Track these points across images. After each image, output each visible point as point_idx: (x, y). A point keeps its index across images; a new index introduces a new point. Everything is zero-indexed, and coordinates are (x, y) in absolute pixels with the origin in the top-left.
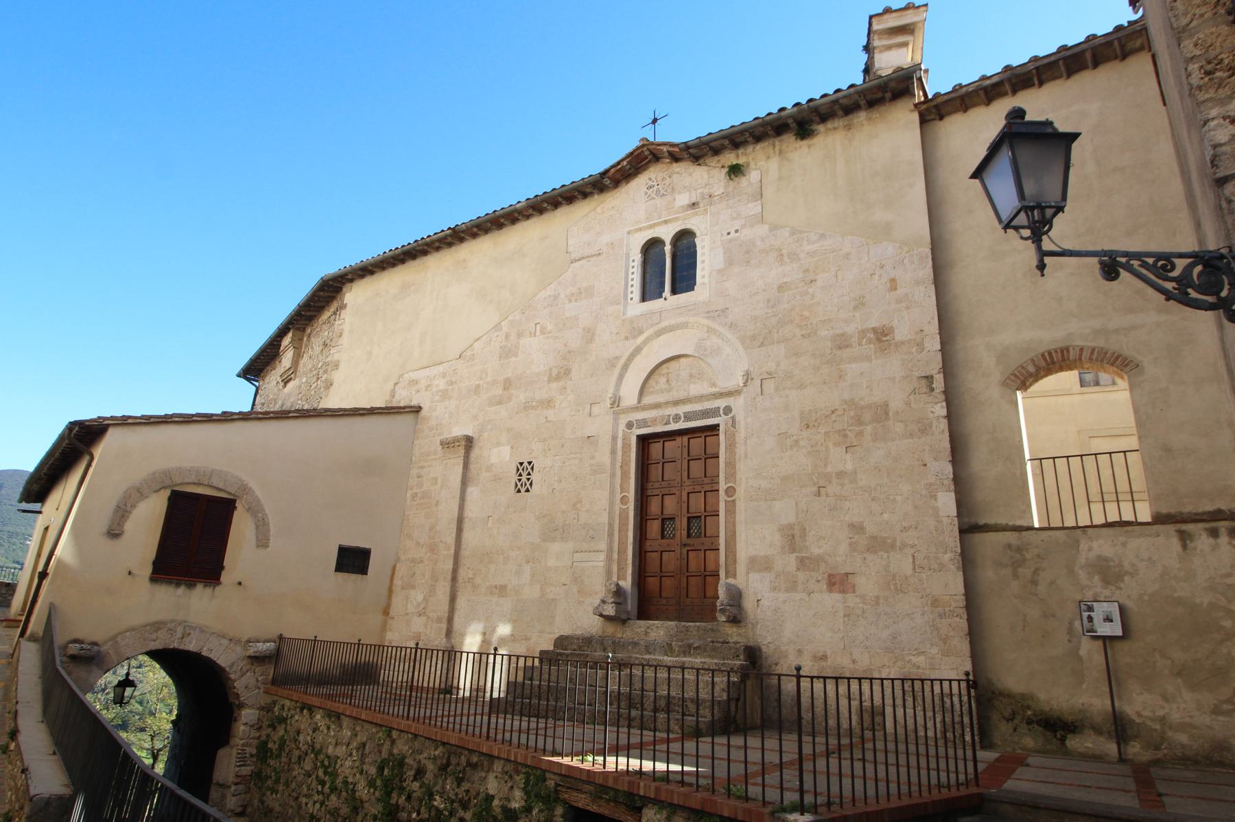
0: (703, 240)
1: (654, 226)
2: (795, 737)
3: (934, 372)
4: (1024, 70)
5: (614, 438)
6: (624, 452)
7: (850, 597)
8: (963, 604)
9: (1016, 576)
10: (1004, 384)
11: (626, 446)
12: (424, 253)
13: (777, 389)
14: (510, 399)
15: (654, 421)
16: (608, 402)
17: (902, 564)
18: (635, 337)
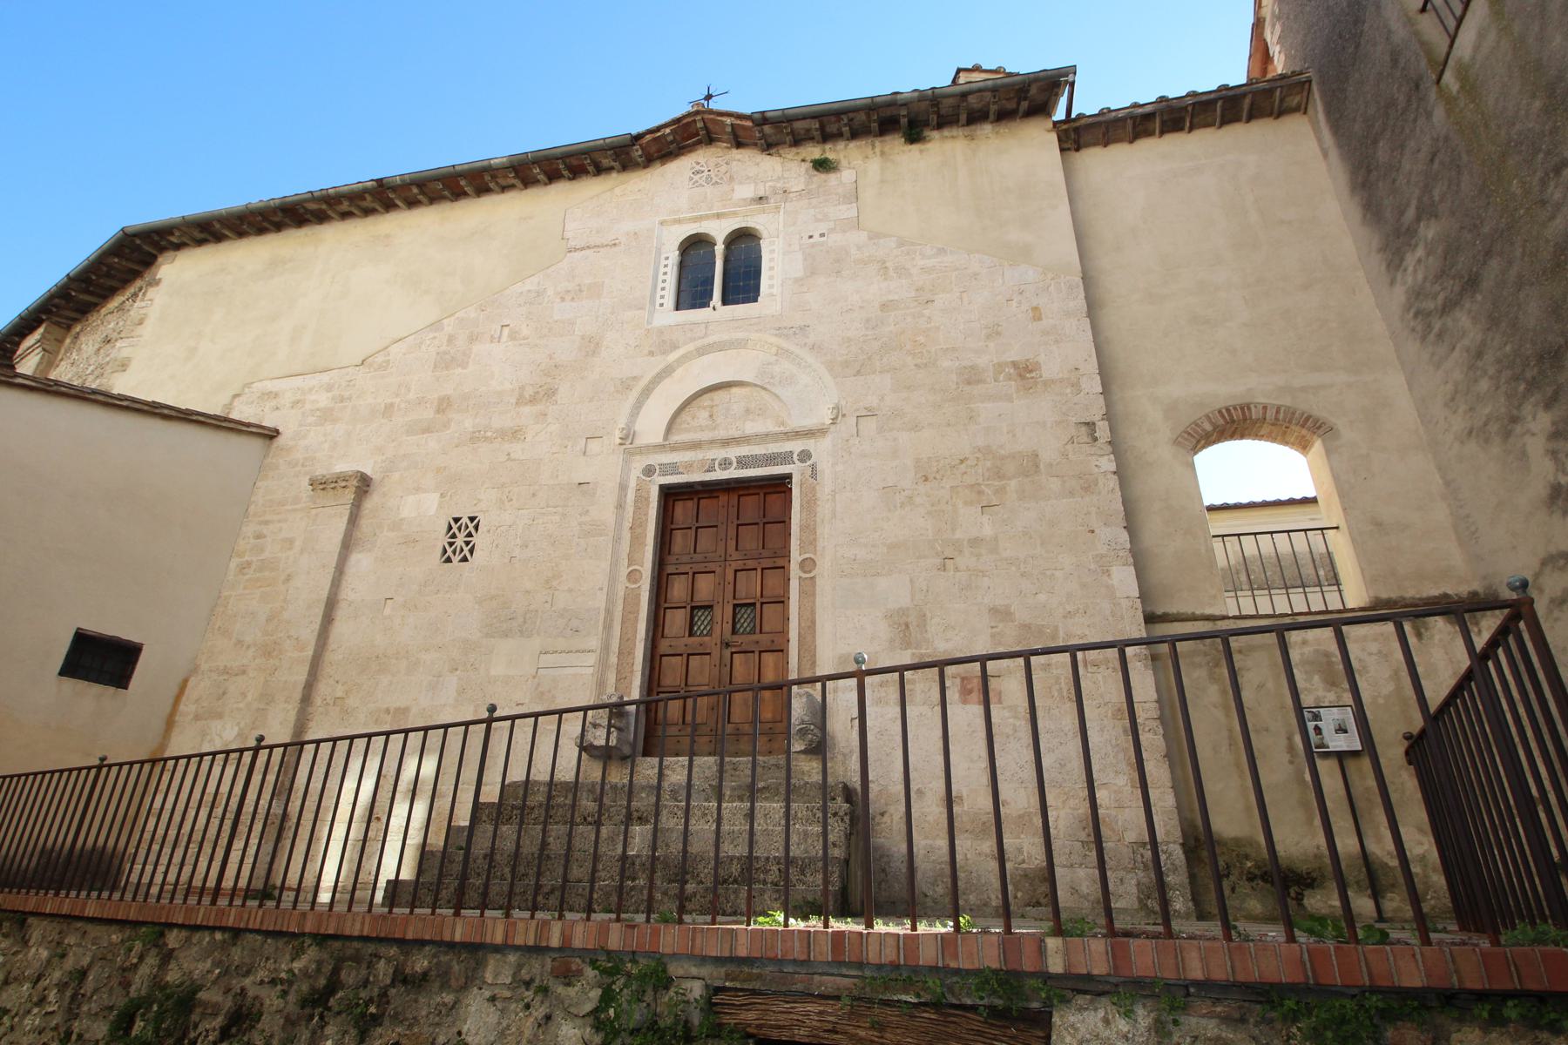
1: (707, 217)
3: (1096, 418)
5: (623, 488)
6: (637, 508)
10: (1176, 442)
11: (641, 499)
12: (321, 218)
14: (446, 425)
15: (689, 466)
16: (618, 434)
18: (664, 353)
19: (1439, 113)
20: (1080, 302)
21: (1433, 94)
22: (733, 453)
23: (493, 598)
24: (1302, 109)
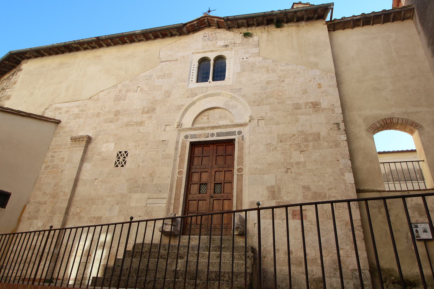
0: (230, 61)
1: (208, 51)
4: (370, 16)
5: (177, 142)
6: (182, 149)
8: (360, 224)
10: (367, 130)
11: (183, 147)
12: (77, 49)
13: (266, 124)
14: (118, 120)
15: (200, 136)
22: (215, 131)
23: (132, 179)
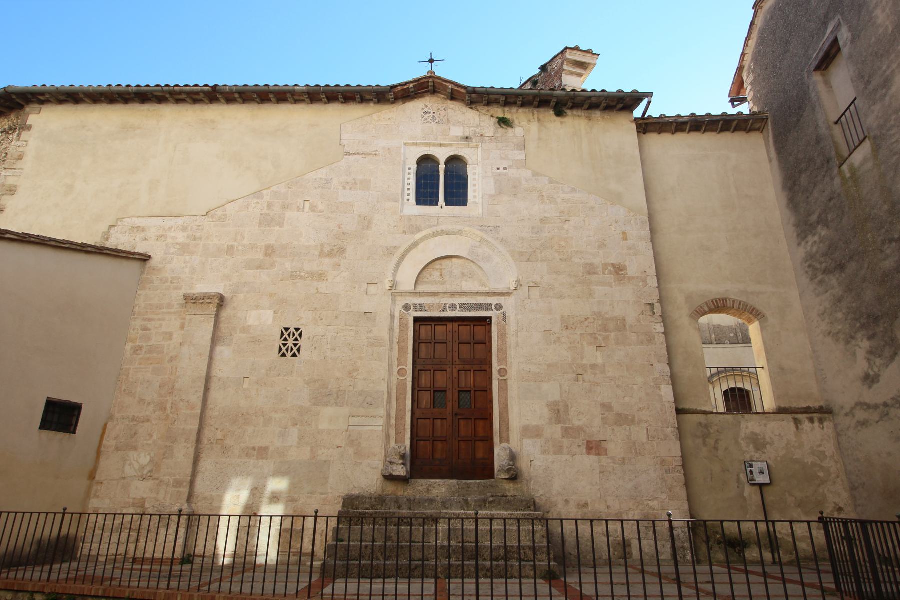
1: (434, 145)
2: (176, 556)
3: (655, 301)
5: (392, 317)
6: (401, 330)
7: (603, 458)
9: (705, 444)
11: (403, 326)
13: (542, 296)
14: (273, 265)
15: (431, 307)
17: (640, 434)
19: (838, 181)
20: (646, 232)
21: (836, 171)
22: (457, 301)
23: (315, 381)
24: (760, 130)
